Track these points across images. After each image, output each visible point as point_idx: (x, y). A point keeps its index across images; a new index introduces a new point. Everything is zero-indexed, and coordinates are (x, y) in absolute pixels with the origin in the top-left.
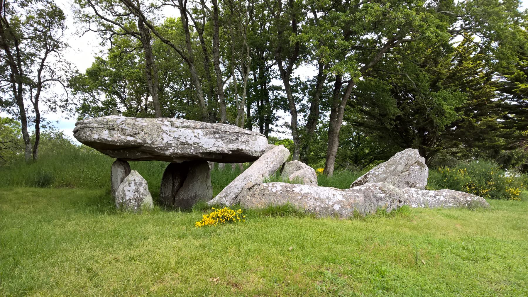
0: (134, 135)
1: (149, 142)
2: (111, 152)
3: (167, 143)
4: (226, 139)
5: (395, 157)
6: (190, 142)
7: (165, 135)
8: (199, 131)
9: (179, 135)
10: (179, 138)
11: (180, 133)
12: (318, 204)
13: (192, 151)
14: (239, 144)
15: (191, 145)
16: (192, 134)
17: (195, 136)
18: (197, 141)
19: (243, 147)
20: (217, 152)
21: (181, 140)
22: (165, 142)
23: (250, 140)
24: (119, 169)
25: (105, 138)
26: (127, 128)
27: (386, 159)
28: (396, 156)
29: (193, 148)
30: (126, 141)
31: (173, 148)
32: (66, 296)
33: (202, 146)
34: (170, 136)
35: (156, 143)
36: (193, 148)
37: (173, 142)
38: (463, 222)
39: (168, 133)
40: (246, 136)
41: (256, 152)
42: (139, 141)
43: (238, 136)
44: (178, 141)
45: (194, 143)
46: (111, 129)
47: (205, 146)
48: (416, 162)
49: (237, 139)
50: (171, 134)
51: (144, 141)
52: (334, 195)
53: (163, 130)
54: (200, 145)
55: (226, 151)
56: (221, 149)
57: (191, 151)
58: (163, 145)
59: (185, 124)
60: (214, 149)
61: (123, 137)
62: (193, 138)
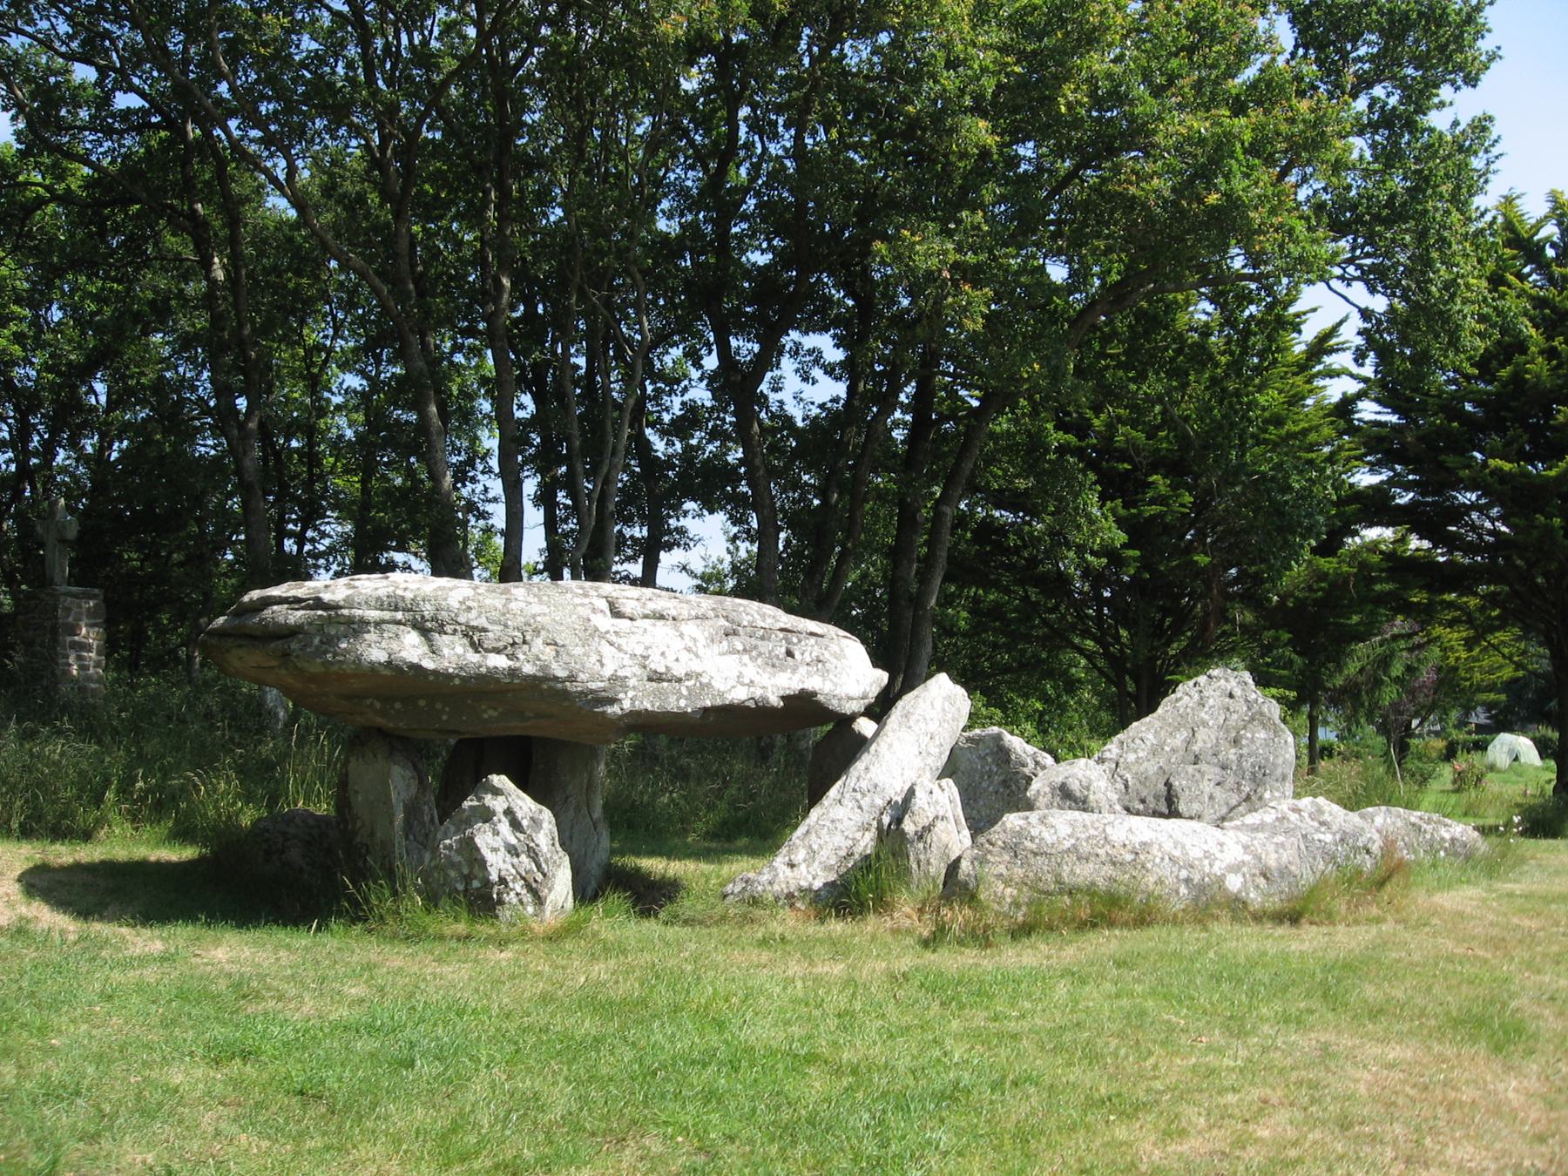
0: (510, 648)
1: (561, 674)
2: (378, 705)
3: (614, 678)
4: (760, 654)
5: (1178, 700)
6: (679, 671)
7: (607, 650)
8: (690, 629)
9: (647, 648)
10: (645, 658)
11: (647, 640)
12: (1184, 874)
13: (683, 703)
14: (803, 670)
15: (679, 680)
16: (678, 644)
17: (689, 650)
18: (696, 666)
19: (813, 683)
20: (752, 704)
21: (653, 666)
22: (608, 672)
23: (827, 655)
24: (397, 771)
25: (415, 661)
26: (487, 625)
27: (1151, 708)
28: (1178, 694)
29: (685, 692)
30: (483, 670)
31: (631, 694)
32: (1562, 1098)
33: (709, 685)
34: (619, 649)
35: (582, 676)
36: (685, 692)
37: (632, 671)
38: (87, 956)
39: (613, 638)
40: (812, 640)
41: (850, 698)
42: (528, 669)
43: (789, 642)
44: (645, 667)
45: (688, 676)
46: (426, 628)
47: (718, 685)
48: (1253, 719)
49: (790, 654)
50: (622, 641)
51: (544, 668)
52: (1221, 845)
53: (597, 630)
54: (704, 680)
55: (775, 701)
56: (758, 693)
57: (678, 701)
58: (601, 685)
59: (651, 606)
60: (739, 695)
61: (473, 658)
62: (684, 656)
